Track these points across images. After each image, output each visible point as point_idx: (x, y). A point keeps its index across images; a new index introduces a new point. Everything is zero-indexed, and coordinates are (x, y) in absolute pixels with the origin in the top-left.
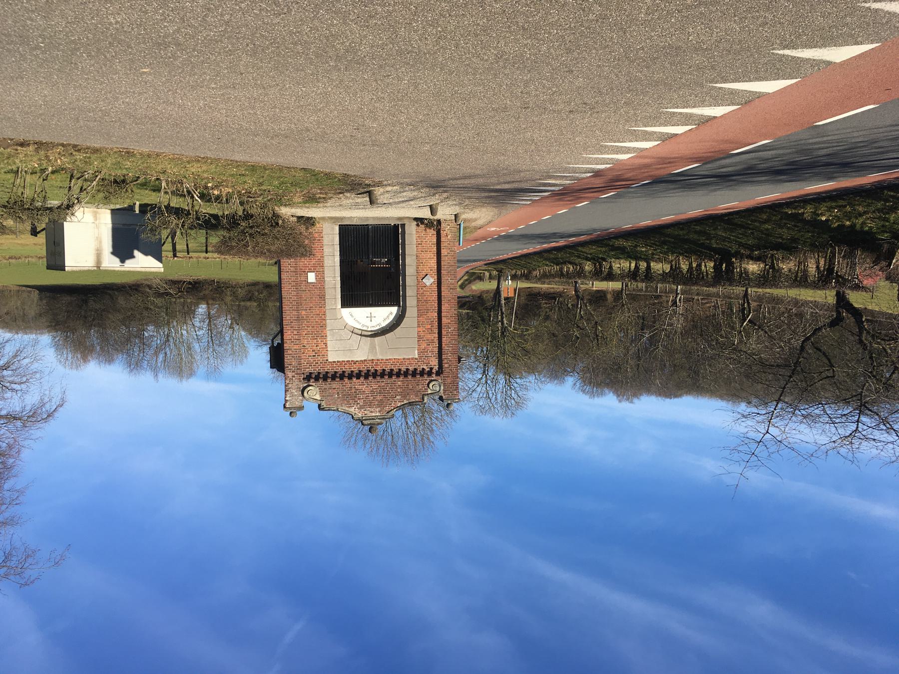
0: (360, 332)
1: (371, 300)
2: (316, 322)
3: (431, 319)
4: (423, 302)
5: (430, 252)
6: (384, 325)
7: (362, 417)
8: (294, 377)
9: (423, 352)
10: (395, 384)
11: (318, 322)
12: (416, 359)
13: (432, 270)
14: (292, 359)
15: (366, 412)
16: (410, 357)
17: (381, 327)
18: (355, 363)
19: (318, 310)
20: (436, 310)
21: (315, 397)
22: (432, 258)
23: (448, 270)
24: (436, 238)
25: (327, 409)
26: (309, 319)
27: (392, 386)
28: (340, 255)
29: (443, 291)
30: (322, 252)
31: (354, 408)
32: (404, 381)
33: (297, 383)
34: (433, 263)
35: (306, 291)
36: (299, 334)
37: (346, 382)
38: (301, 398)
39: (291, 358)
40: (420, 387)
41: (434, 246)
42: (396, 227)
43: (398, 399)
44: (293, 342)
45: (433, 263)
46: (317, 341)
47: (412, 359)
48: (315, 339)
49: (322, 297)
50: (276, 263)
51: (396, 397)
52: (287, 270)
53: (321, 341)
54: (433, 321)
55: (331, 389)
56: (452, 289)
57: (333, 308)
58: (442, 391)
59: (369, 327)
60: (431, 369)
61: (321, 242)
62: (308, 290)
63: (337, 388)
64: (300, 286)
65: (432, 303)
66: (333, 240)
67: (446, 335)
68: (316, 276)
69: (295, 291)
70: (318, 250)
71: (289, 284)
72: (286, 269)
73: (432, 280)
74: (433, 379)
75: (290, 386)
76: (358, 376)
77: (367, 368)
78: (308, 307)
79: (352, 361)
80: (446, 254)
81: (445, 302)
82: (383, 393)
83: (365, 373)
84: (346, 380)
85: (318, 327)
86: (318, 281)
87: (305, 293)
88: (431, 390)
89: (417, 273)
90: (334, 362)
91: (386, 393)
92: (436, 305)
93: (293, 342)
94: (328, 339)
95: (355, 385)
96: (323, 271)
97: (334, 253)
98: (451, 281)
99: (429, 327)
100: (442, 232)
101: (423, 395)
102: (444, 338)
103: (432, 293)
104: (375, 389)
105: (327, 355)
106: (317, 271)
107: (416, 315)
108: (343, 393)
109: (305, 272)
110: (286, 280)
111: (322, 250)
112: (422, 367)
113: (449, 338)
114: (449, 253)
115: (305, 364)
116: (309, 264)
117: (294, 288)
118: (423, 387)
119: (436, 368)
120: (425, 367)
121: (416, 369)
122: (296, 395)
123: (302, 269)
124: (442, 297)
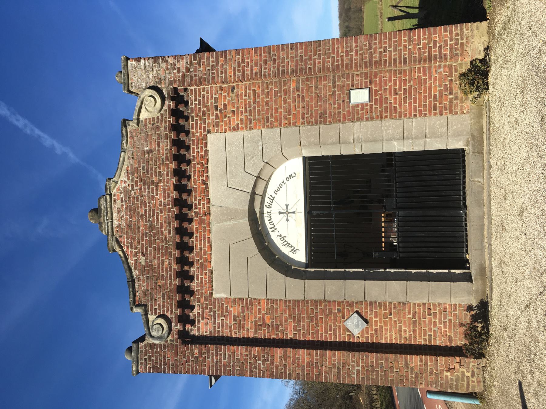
0: (259, 191)
1: (319, 213)
2: (276, 109)
3: (282, 325)
4: (313, 313)
5: (414, 331)
6: (272, 238)
7: (110, 195)
8: (179, 71)
9: (222, 309)
11: (276, 112)
12: (211, 294)
13: (376, 333)
14: (208, 65)
15: (119, 201)
16: (214, 284)
17: (270, 230)
18: (203, 182)
19: (299, 111)
20: (300, 336)
21: (143, 109)
22: (400, 335)
23: (377, 367)
24: (444, 345)
25: (124, 132)
26: (281, 96)
27: (162, 249)
29: (334, 355)
30: (411, 115)
31: (126, 180)
32: (170, 271)
33: (168, 77)
34: (391, 335)
35: (334, 87)
36: (254, 76)
37: (170, 165)
38: (144, 85)
39: (211, 64)
40: (160, 301)
41: (425, 340)
42: (463, 264)
43: (139, 259)
44: (239, 67)
45: (391, 335)
46: (242, 112)
47: (211, 287)
48: (246, 109)
51: (143, 255)
52: (374, 46)
53: (242, 120)
54: (278, 330)
55: (158, 139)
56: (339, 373)
57: (301, 139)
58: (151, 341)
59: (269, 210)
60: (193, 323)
62: (335, 91)
63: (159, 150)
64: (343, 75)
65: (313, 329)
66: (435, 135)
67: (250, 356)
68: (362, 104)
69: (333, 63)
70: (415, 107)
71: (347, 51)
72: (375, 44)
73: (356, 332)
74: (173, 324)
75: (164, 65)
76: (180, 188)
77: (196, 204)
78: (303, 93)
79: (208, 177)
80: (411, 365)
81: (312, 357)
82: (150, 232)
83: (186, 200)
84: (173, 166)
85: (267, 113)
86: (353, 109)
87: (329, 86)
88: (154, 321)
89: (371, 303)
90: (206, 145)
91: (150, 238)
92: (308, 337)
93: (239, 67)
94: (247, 133)
95: (164, 182)
96: (372, 118)
97: (408, 138)
99: (268, 322)
100: (458, 359)
101: (146, 305)
102: (246, 350)
103: (330, 330)
104: (157, 218)
105: (217, 131)
106: (371, 106)
107: (290, 297)
108: (152, 160)
109: (371, 82)
110: (354, 44)
111: (415, 116)
112: (196, 304)
113: (246, 360)
114: (412, 372)
115: (202, 93)
116: (386, 90)
117: (338, 61)
118: (159, 306)
119: (194, 331)
120: (196, 311)
121: (192, 293)
122: (147, 76)
123: (376, 76)
124: (323, 352)
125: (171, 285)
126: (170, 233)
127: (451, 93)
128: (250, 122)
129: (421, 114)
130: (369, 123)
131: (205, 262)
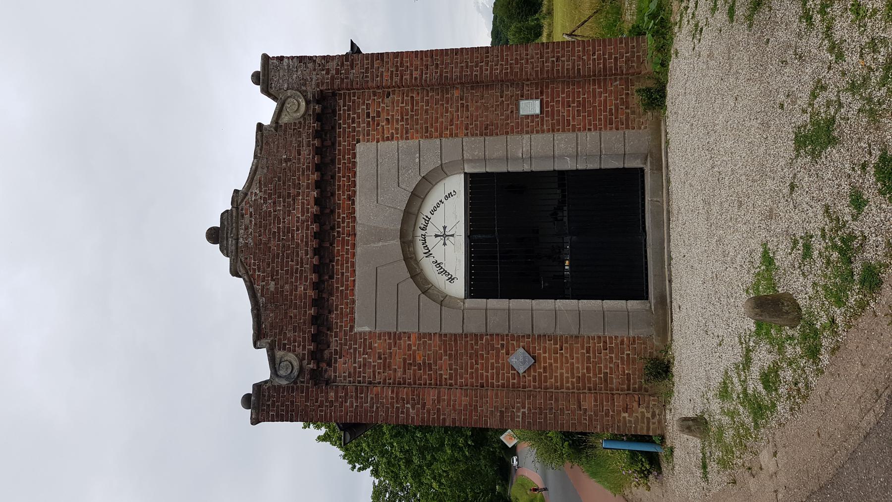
2: (437, 118)
8: (328, 73)
9: (365, 345)
10: (301, 279)
12: (352, 328)
13: (545, 371)
18: (349, 198)
22: (573, 374)
28: (577, 172)
35: (502, 97)
43: (268, 284)
47: (353, 320)
49: (487, 130)
50: (339, 89)
51: (272, 280)
52: (545, 55)
54: (430, 369)
59: (423, 233)
61: (605, 126)
63: (299, 159)
78: (467, 102)
79: (355, 192)
82: (283, 252)
85: (426, 122)
86: (522, 121)
89: (539, 336)
90: (354, 157)
94: (402, 143)
96: (543, 132)
98: (520, 414)
99: (419, 361)
104: (293, 237)
109: (542, 93)
111: (590, 130)
113: (392, 404)
125: (305, 314)
126: (307, 254)
127: (627, 108)
128: (407, 133)
129: (595, 129)
130: (540, 136)
131: (347, 289)
